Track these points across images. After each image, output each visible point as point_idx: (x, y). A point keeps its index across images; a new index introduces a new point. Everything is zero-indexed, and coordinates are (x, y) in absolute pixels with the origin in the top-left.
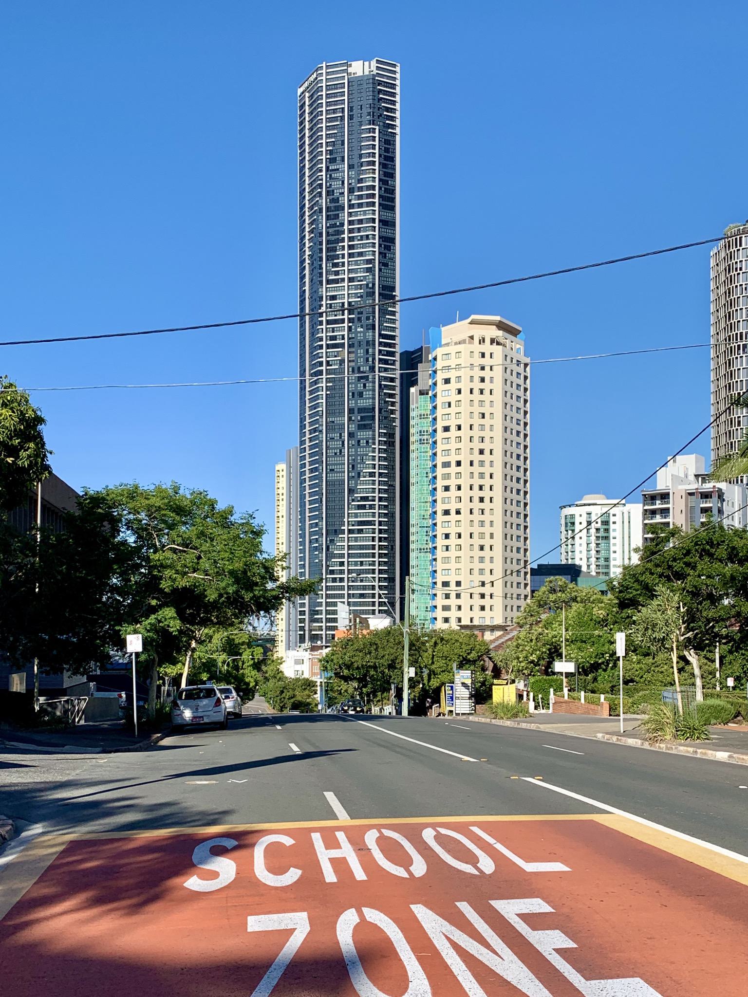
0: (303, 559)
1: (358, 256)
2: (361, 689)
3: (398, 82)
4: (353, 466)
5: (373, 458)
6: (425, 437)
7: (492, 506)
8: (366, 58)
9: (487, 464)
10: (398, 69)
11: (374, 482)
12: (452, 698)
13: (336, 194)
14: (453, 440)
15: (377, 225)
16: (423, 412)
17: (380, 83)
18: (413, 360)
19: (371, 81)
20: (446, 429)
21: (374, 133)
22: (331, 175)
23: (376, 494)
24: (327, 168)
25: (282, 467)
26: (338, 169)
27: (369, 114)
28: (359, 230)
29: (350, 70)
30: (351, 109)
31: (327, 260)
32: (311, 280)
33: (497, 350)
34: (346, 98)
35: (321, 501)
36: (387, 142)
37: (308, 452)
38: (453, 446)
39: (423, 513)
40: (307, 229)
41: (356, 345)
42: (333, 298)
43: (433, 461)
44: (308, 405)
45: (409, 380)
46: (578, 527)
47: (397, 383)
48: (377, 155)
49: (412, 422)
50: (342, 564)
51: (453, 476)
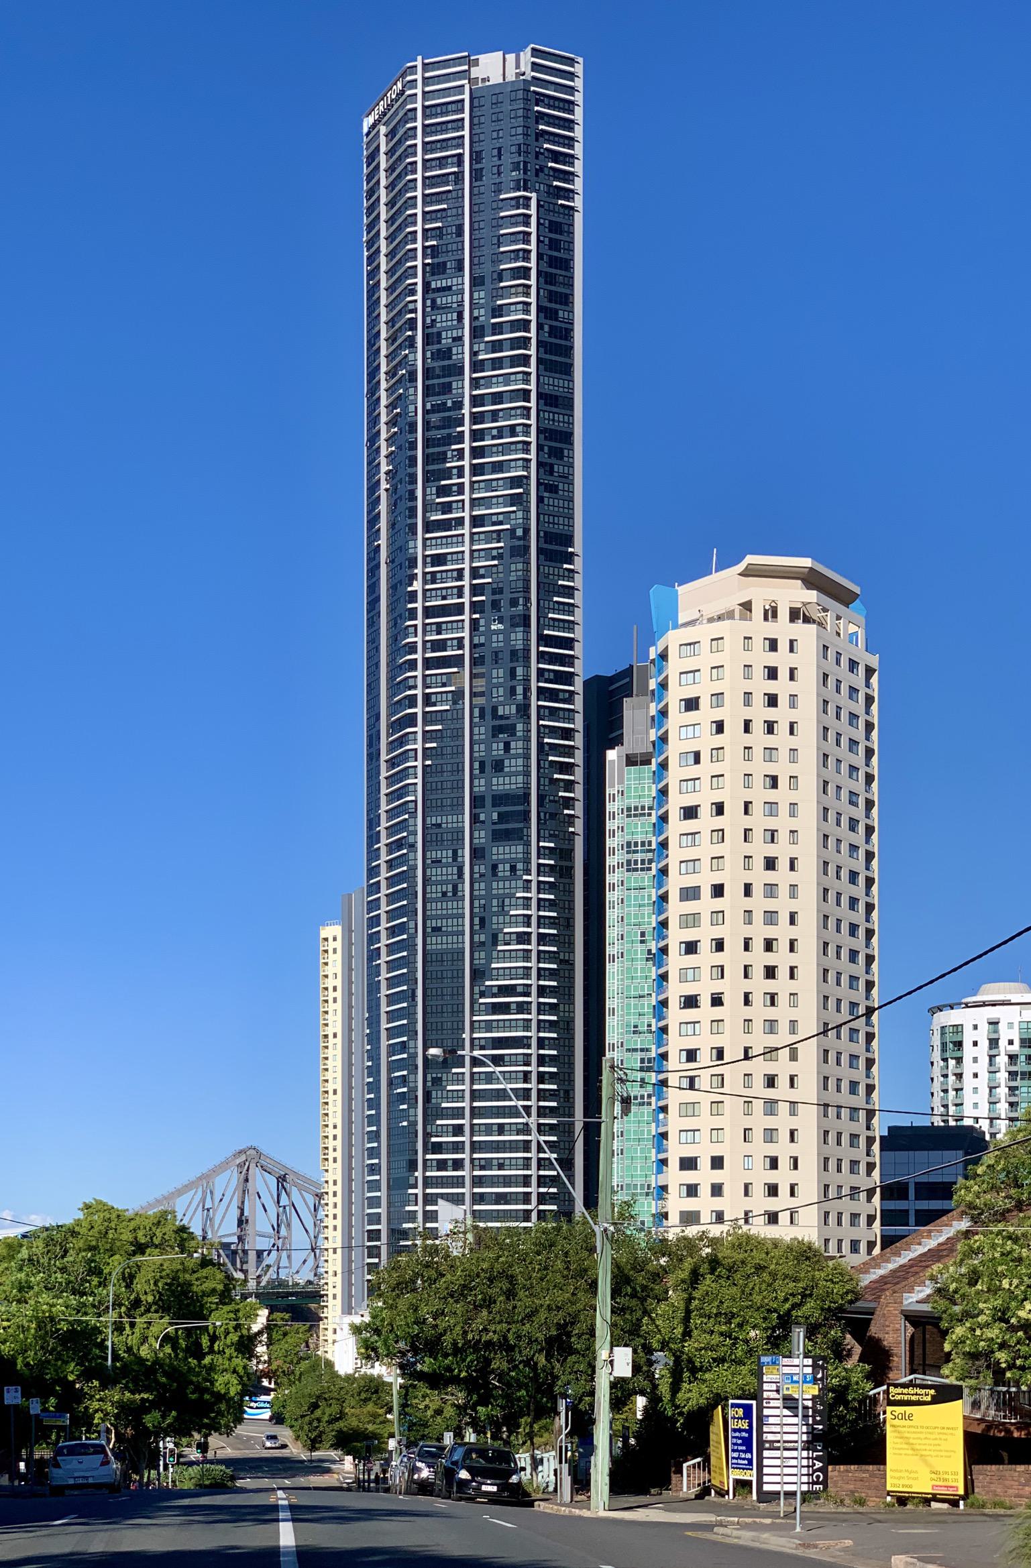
0: (374, 1120)
1: (493, 472)
2: (474, 1409)
3: (578, 98)
4: (482, 920)
5: (526, 903)
6: (639, 857)
7: (793, 986)
8: (510, 46)
9: (783, 891)
10: (578, 69)
11: (526, 955)
12: (747, 1442)
13: (446, 342)
14: (705, 836)
15: (533, 404)
16: (633, 803)
17: (540, 99)
18: (608, 701)
19: (520, 94)
20: (690, 813)
21: (528, 207)
22: (434, 301)
23: (533, 981)
24: (426, 285)
25: (332, 931)
26: (449, 288)
27: (516, 167)
28: (495, 415)
29: (475, 72)
30: (476, 157)
31: (426, 480)
32: (392, 525)
33: (807, 634)
34: (466, 133)
35: (414, 996)
36: (555, 227)
37: (384, 891)
38: (705, 849)
39: (633, 1020)
40: (384, 418)
41: (488, 660)
42: (439, 560)
43: (660, 886)
44: (384, 790)
45: (605, 726)
46: (968, 1051)
47: (578, 741)
48: (533, 256)
49: (610, 825)
50: (458, 1130)
51: (705, 919)
